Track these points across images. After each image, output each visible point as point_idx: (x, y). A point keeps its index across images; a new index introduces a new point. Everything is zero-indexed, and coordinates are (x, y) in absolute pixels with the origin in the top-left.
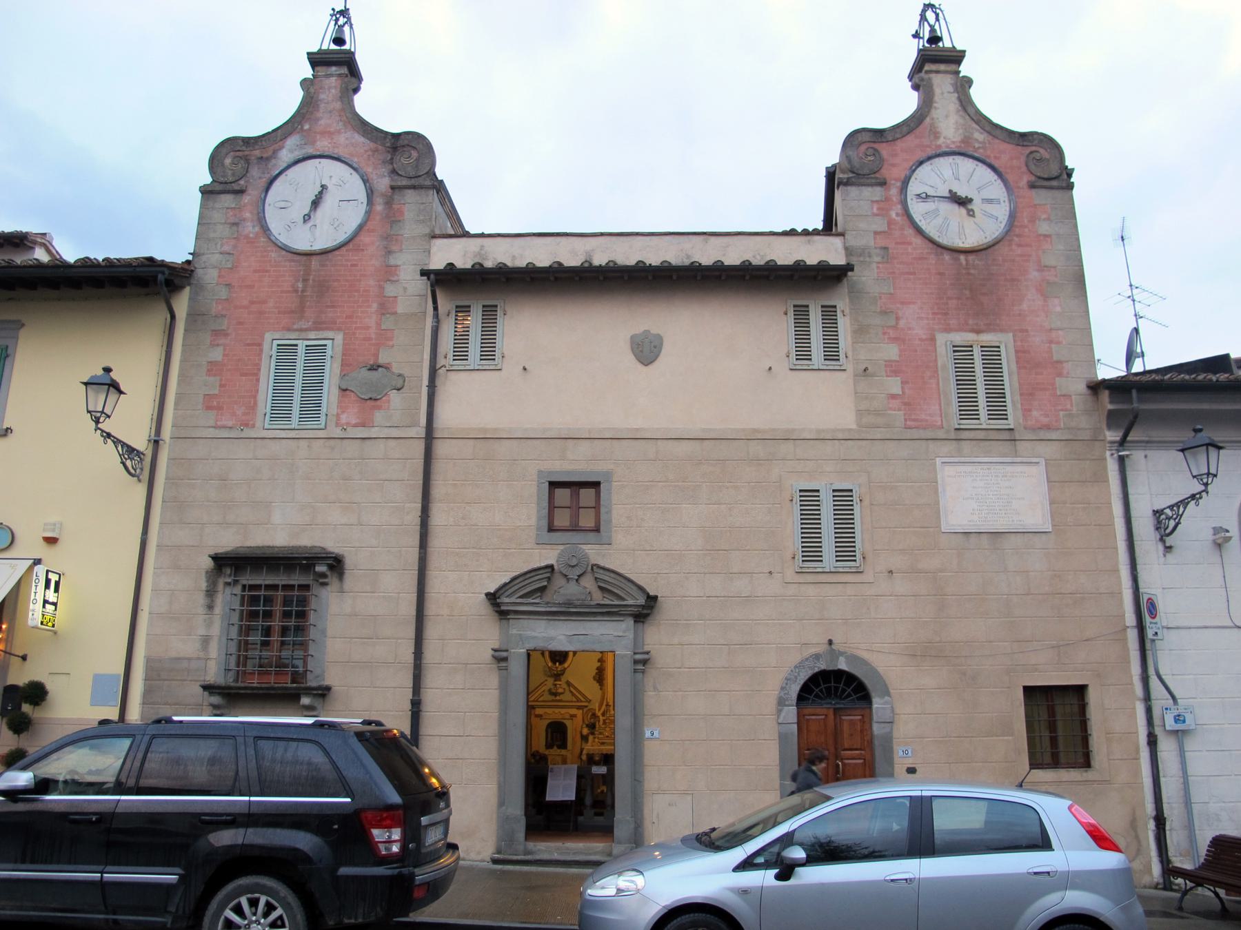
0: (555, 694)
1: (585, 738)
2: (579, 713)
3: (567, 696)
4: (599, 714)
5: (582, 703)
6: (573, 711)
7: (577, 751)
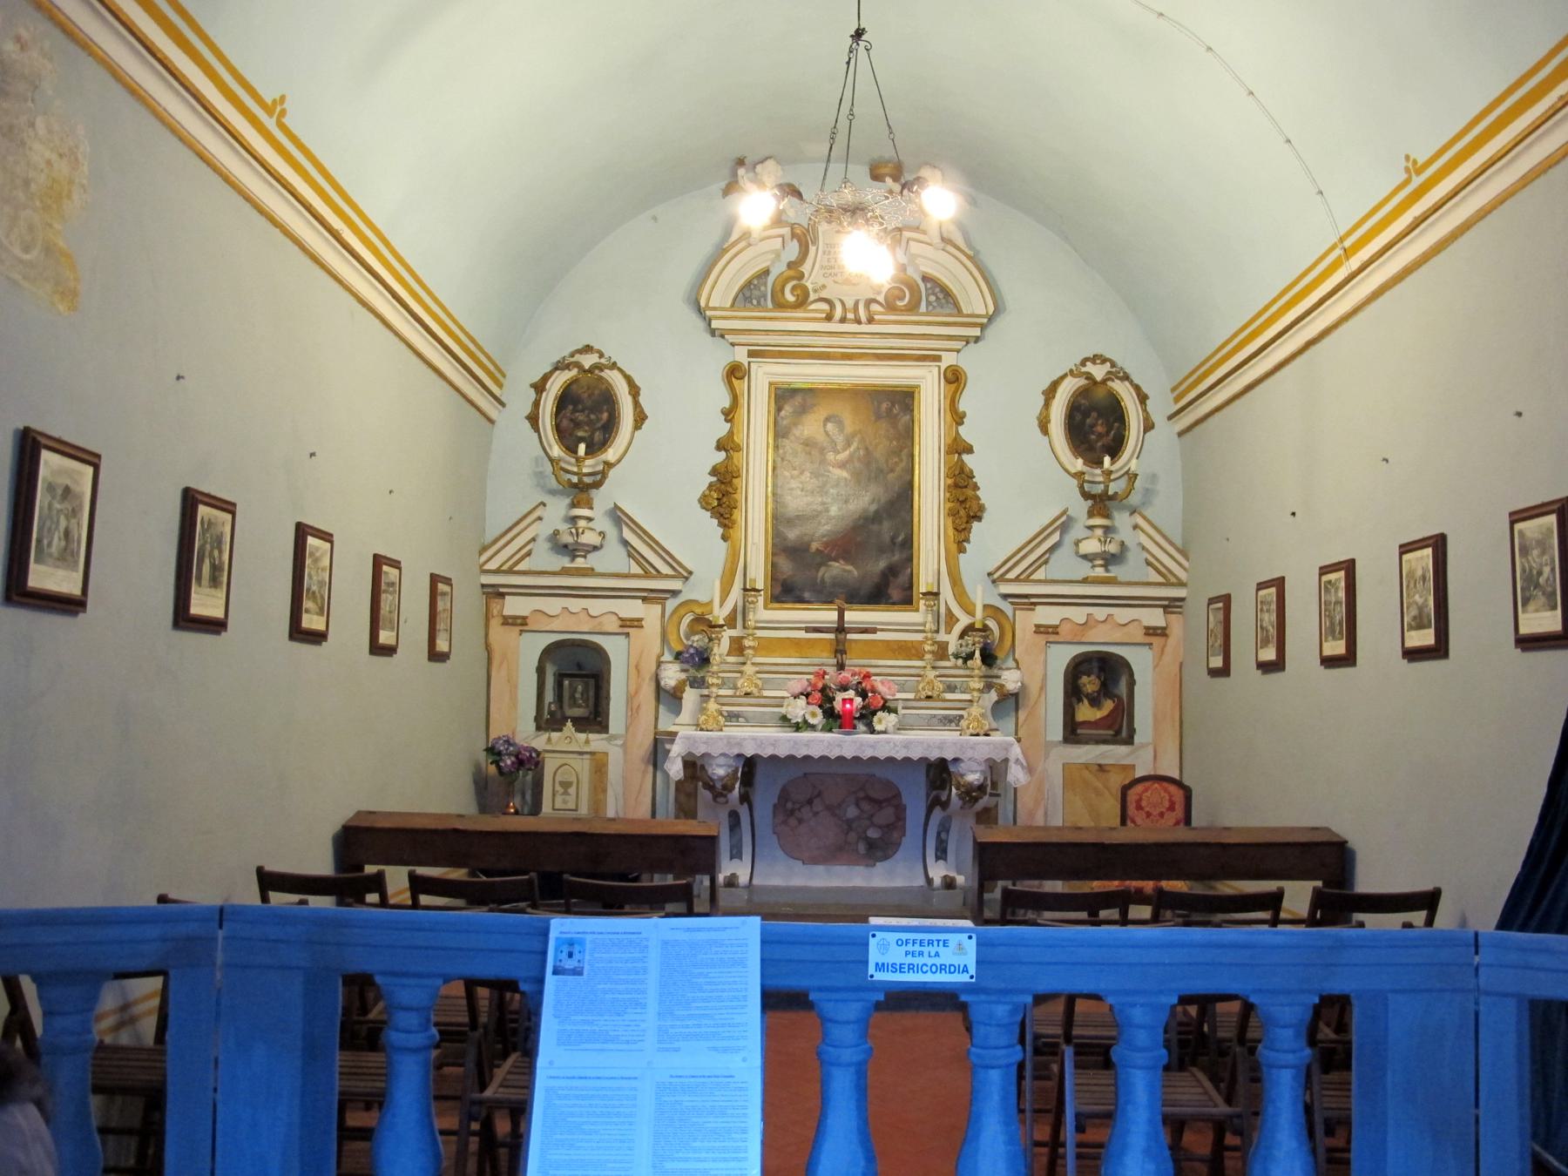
0: (570, 550)
1: (669, 698)
2: (651, 614)
3: (611, 559)
4: (720, 614)
5: (657, 575)
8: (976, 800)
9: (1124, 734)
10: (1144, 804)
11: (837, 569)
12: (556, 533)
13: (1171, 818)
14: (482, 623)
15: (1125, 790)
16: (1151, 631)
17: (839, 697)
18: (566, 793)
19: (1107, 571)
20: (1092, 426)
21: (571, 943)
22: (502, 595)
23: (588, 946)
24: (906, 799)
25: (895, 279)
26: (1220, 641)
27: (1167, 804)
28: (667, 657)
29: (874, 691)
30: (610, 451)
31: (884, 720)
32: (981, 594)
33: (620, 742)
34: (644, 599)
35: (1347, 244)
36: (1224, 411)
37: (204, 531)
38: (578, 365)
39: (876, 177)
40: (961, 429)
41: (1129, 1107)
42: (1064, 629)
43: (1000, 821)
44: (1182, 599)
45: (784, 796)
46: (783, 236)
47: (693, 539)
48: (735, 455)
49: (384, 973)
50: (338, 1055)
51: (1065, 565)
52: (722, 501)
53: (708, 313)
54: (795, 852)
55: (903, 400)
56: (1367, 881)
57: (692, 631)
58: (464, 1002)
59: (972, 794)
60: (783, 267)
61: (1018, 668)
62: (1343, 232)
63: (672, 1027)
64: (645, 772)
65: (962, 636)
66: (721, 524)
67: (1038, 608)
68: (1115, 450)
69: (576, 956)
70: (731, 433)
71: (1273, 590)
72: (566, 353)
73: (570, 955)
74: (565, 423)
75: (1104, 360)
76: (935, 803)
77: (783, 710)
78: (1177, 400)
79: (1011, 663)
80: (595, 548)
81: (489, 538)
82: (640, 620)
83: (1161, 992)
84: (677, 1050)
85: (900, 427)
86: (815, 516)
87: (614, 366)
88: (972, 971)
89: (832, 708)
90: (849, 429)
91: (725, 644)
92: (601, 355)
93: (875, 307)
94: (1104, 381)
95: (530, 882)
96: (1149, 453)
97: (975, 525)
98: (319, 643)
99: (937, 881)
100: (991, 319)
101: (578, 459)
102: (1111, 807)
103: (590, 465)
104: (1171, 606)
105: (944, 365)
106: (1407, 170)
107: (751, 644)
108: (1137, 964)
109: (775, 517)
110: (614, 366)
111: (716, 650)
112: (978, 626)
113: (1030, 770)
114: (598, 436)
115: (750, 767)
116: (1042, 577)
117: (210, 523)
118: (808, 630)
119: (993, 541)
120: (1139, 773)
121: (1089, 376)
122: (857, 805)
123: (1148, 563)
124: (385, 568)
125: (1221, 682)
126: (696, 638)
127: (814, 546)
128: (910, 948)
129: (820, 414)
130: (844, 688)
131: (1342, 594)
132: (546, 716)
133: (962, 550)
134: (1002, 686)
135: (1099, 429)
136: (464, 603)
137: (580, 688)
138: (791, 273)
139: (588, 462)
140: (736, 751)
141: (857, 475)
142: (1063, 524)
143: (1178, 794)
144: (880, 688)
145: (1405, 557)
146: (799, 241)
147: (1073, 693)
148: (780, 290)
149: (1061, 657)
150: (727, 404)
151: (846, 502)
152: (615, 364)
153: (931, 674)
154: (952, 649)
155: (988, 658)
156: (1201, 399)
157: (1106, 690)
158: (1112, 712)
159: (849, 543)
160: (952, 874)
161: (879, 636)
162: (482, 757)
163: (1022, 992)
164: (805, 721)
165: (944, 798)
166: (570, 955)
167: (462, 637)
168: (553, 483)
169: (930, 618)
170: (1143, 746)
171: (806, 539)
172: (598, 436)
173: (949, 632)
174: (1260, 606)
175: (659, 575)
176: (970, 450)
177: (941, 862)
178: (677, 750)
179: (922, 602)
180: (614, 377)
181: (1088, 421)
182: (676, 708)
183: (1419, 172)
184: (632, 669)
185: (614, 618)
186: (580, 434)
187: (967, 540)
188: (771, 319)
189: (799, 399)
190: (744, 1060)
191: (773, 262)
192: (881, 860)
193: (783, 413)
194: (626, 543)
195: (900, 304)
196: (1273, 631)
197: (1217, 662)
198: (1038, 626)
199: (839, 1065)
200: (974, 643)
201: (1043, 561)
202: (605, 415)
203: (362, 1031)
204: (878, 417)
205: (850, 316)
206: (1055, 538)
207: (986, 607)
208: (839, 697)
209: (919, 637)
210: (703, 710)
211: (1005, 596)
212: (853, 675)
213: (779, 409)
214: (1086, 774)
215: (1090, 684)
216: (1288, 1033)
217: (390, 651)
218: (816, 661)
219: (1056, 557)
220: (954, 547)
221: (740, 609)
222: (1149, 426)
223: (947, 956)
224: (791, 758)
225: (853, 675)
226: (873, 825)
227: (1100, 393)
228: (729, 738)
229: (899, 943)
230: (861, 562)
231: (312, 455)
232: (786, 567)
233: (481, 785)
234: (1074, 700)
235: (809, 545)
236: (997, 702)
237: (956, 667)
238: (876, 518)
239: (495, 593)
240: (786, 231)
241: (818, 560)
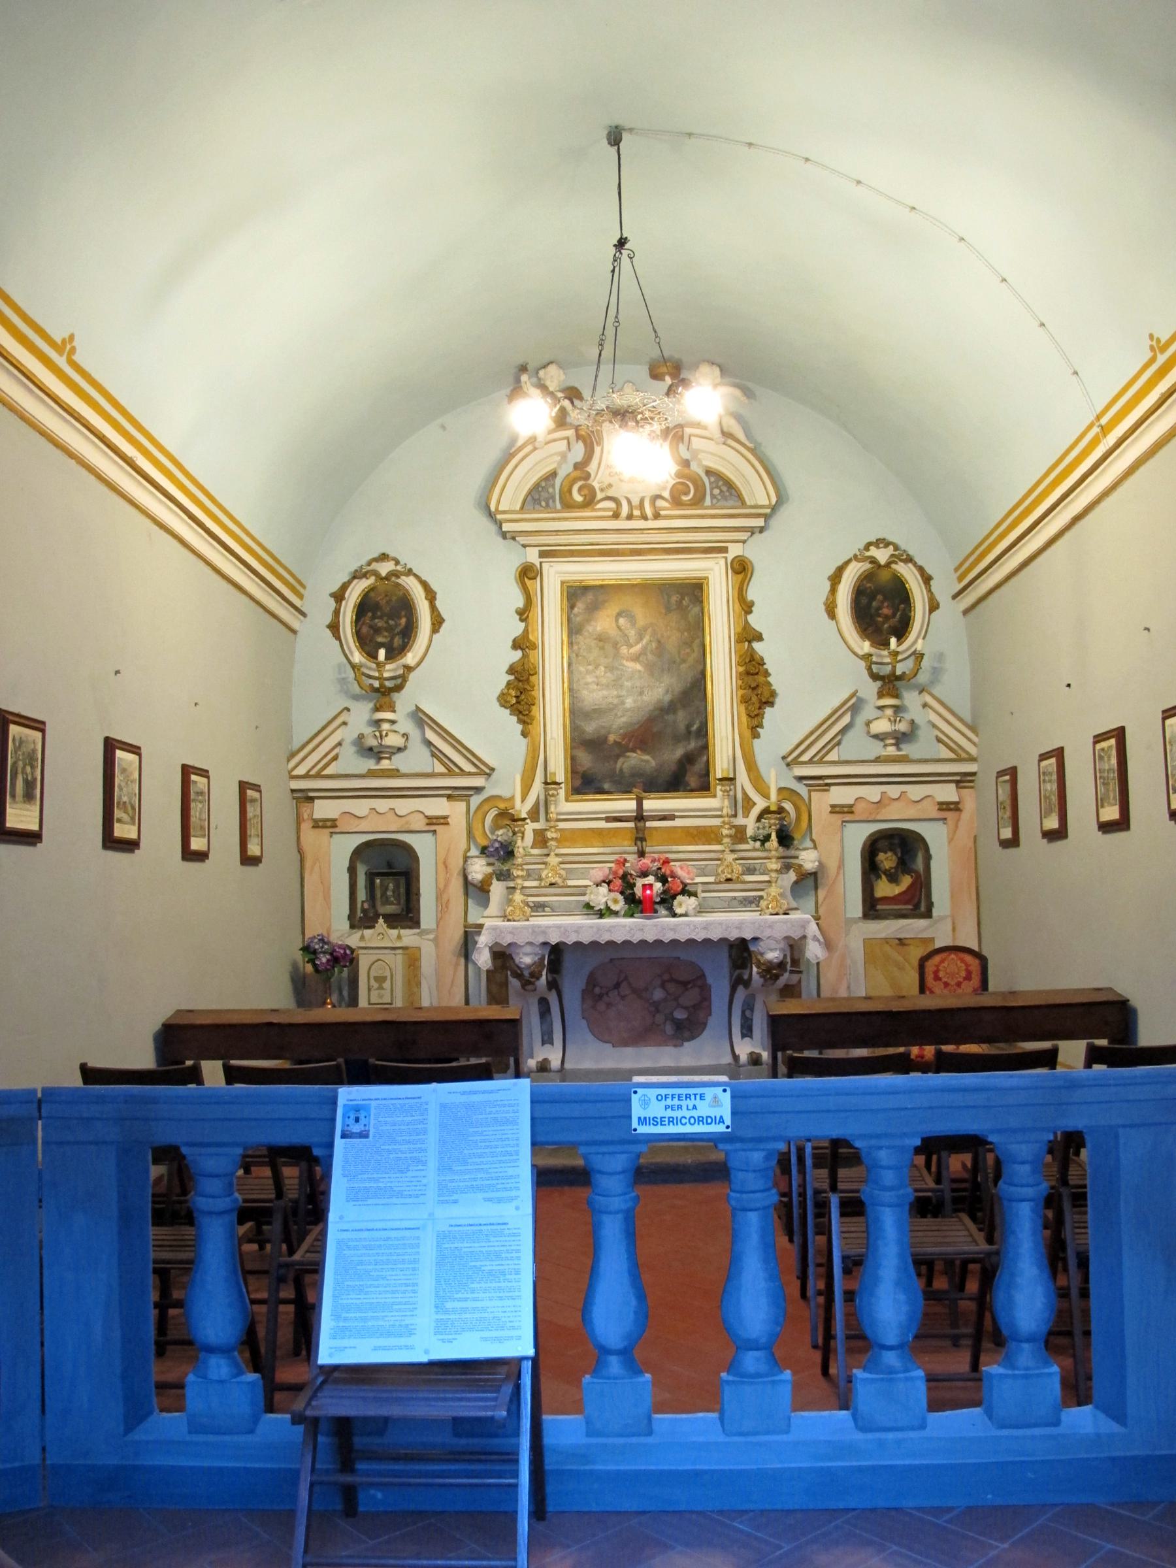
0: (376, 753)
1: (478, 891)
2: (456, 811)
3: (416, 760)
4: (522, 809)
5: (462, 775)
6: (437, 807)
7: (455, 935)
8: (777, 977)
9: (923, 908)
10: (941, 974)
11: (636, 760)
12: (361, 737)
13: (968, 987)
14: (294, 826)
15: (923, 961)
16: (945, 806)
17: (640, 882)
18: (381, 988)
19: (899, 749)
20: (879, 608)
21: (357, 1109)
22: (312, 799)
23: (373, 1112)
24: (710, 980)
25: (679, 475)
26: (1008, 813)
27: (963, 974)
28: (474, 852)
29: (673, 876)
30: (410, 655)
31: (684, 904)
32: (775, 777)
33: (431, 936)
34: (449, 797)
35: (1104, 421)
36: (1004, 588)
37: (16, 750)
38: (376, 573)
39: (655, 376)
40: (750, 618)
41: (880, 1242)
42: (858, 809)
43: (804, 995)
44: (974, 774)
45: (592, 981)
46: (568, 439)
47: (494, 738)
48: (531, 653)
49: (187, 1144)
50: (151, 1228)
51: (857, 745)
52: (520, 695)
53: (499, 517)
54: (602, 1033)
55: (694, 590)
56: (1149, 1035)
57: (496, 826)
58: (271, 1182)
59: (772, 971)
60: (571, 468)
61: (815, 847)
62: (1099, 409)
63: (452, 1181)
64: (457, 965)
65: (759, 819)
66: (520, 721)
67: (833, 788)
68: (901, 631)
69: (363, 1121)
70: (526, 631)
71: (1053, 760)
72: (363, 561)
73: (357, 1120)
74: (365, 630)
75: (887, 544)
76: (739, 982)
77: (586, 898)
78: (960, 579)
79: (808, 844)
80: (400, 750)
81: (296, 745)
82: (446, 817)
83: (905, 1135)
84: (456, 1202)
85: (690, 619)
86: (611, 709)
87: (410, 572)
88: (728, 1121)
89: (634, 894)
90: (641, 622)
91: (529, 837)
92: (397, 563)
93: (660, 503)
94: (888, 565)
95: (338, 1066)
96: (935, 633)
97: (768, 710)
98: (131, 851)
99: (744, 1058)
100: (774, 509)
101: (379, 665)
102: (913, 977)
103: (390, 670)
104: (963, 781)
105: (731, 556)
106: (1152, 348)
107: (554, 835)
108: (887, 1110)
109: (573, 712)
110: (410, 572)
111: (519, 843)
112: (773, 808)
113: (828, 945)
114: (397, 641)
115: (556, 954)
116: (836, 759)
117: (21, 742)
118: (608, 819)
119: (785, 725)
120: (939, 944)
121: (873, 561)
122: (663, 986)
123: (939, 740)
124: (193, 777)
125: (1012, 851)
126: (500, 832)
127: (612, 738)
128: (669, 1102)
129: (611, 610)
130: (644, 874)
131: (1114, 761)
132: (359, 914)
133: (756, 736)
134: (800, 866)
135: (886, 611)
136: (274, 809)
137: (391, 886)
138: (578, 473)
139: (388, 667)
140: (542, 940)
141: (650, 668)
142: (854, 705)
143: (974, 963)
144: (680, 872)
145: (1168, 722)
146: (585, 442)
147: (871, 868)
148: (566, 491)
149: (857, 835)
150: (520, 603)
151: (641, 693)
152: (410, 570)
153: (730, 857)
154: (750, 832)
155: (785, 839)
156: (984, 576)
157: (904, 865)
158: (909, 888)
159: (644, 735)
160: (757, 1051)
161: (678, 823)
162: (299, 956)
163: (775, 1139)
164: (608, 908)
165: (746, 977)
166: (357, 1120)
167: (273, 839)
168: (356, 689)
169: (726, 803)
170: (941, 918)
171: (603, 732)
172: (397, 641)
173: (746, 815)
174: (1042, 774)
175: (463, 773)
176: (759, 638)
177: (747, 1039)
178: (484, 940)
179: (719, 788)
180: (411, 583)
181: (874, 604)
182: (485, 902)
183: (1163, 349)
184: (441, 866)
185: (422, 816)
186: (380, 639)
187: (761, 726)
188: (559, 519)
189: (590, 597)
190: (517, 1208)
191: (560, 464)
192: (688, 1040)
193: (576, 610)
194: (429, 744)
195: (685, 498)
196: (1054, 799)
197: (1007, 833)
198: (833, 806)
199: (610, 1213)
200: (771, 826)
201: (836, 742)
202: (403, 621)
203: (173, 1209)
204: (668, 610)
205: (637, 513)
206: (846, 719)
207: (781, 790)
208: (640, 882)
209: (716, 822)
210: (510, 902)
211: (800, 779)
212: (653, 861)
213: (572, 607)
214: (887, 948)
215: (887, 860)
216: (1026, 1169)
217: (201, 856)
218: (617, 849)
219: (850, 734)
220: (748, 733)
221: (542, 803)
222: (934, 606)
223: (704, 1109)
224: (594, 944)
225: (653, 861)
226: (679, 1006)
227: (885, 576)
228: (533, 926)
229: (659, 1098)
230: (657, 753)
231: (117, 672)
232: (586, 760)
233: (299, 984)
234: (873, 877)
235: (606, 738)
236: (796, 883)
237: (755, 850)
238: (668, 709)
239: (305, 798)
240: (570, 433)
241: (617, 751)
